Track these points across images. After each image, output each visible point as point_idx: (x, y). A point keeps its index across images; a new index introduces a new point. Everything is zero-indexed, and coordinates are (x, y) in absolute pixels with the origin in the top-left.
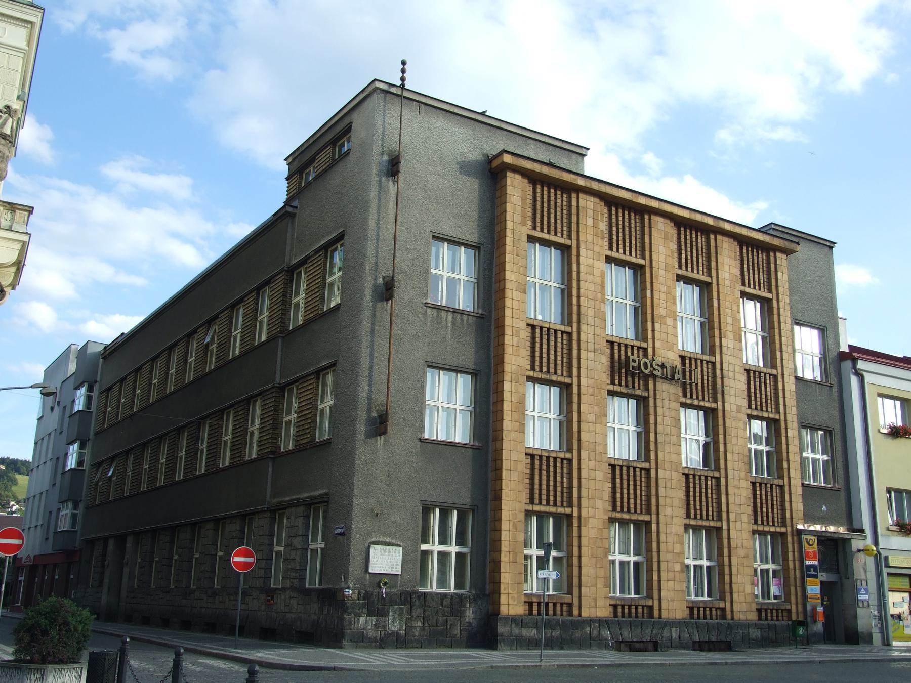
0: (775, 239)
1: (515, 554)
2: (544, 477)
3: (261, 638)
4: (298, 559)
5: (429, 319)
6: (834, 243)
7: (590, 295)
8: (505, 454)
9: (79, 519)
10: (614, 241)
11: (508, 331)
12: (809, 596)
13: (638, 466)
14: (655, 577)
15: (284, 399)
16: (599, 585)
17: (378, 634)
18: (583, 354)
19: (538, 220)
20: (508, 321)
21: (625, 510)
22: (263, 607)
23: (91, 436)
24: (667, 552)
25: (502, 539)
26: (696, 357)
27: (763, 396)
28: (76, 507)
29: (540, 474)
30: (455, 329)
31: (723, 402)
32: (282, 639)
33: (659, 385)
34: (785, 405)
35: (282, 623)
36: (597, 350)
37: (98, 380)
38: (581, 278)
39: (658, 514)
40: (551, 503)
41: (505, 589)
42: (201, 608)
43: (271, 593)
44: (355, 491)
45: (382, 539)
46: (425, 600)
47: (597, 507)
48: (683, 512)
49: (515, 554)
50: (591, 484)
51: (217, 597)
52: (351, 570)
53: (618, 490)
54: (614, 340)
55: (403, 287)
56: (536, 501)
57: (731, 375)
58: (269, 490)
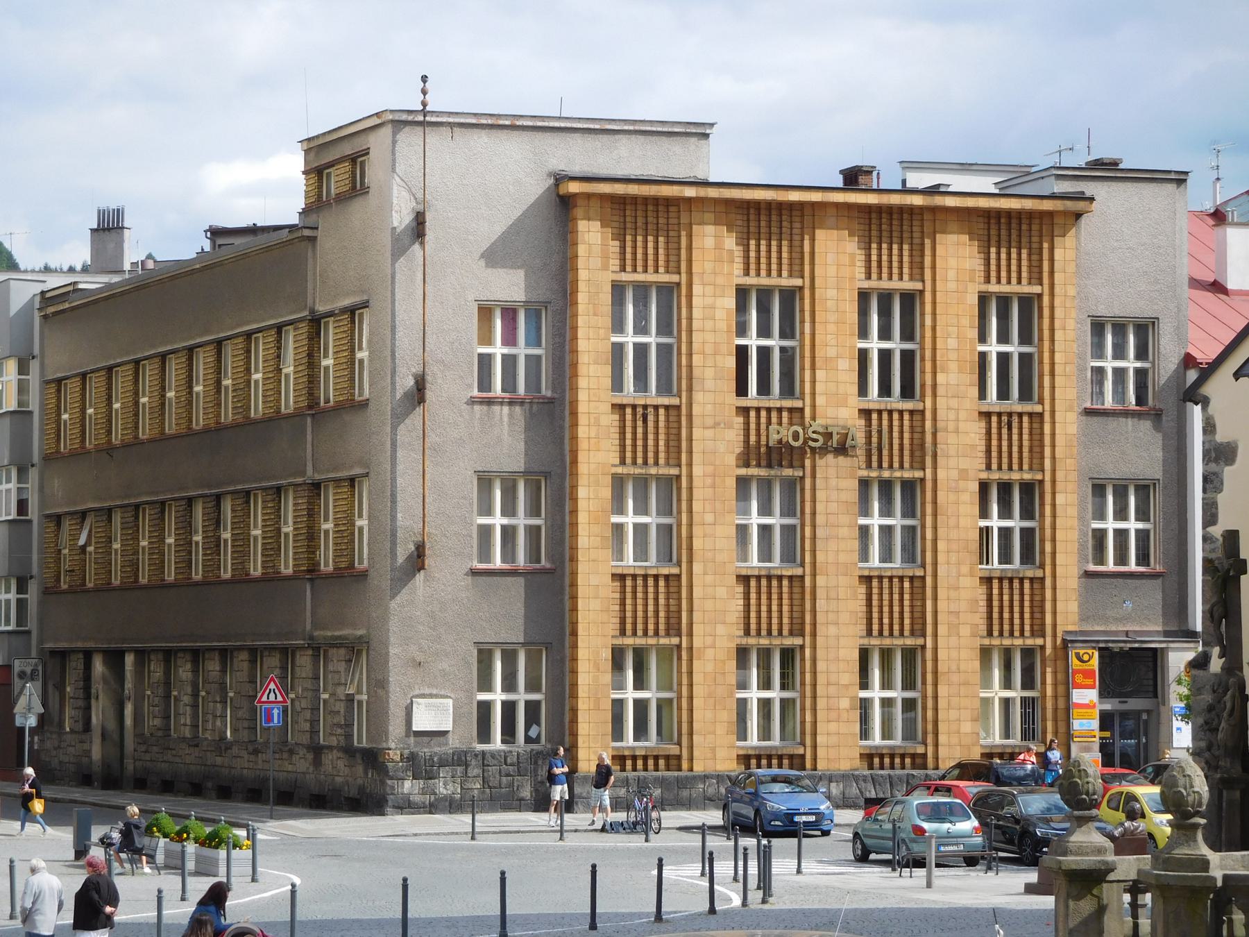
0: (1045, 201)
1: (597, 700)
2: (640, 602)
3: (311, 807)
4: (342, 711)
5: (478, 416)
6: (1186, 173)
7: (709, 349)
8: (581, 580)
9: (33, 608)
10: (752, 260)
11: (582, 419)
12: (1076, 733)
13: (785, 573)
14: (808, 718)
15: (320, 499)
16: (719, 732)
17: (427, 799)
18: (697, 433)
19: (629, 256)
20: (582, 408)
21: (764, 632)
22: (311, 769)
23: (36, 458)
24: (828, 684)
25: (579, 683)
26: (889, 408)
27: (1015, 449)
28: (22, 588)
29: (635, 598)
30: (514, 424)
31: (935, 468)
32: (332, 809)
33: (820, 462)
34: (1053, 458)
35: (330, 788)
36: (719, 424)
37: (36, 351)
38: (694, 328)
39: (814, 635)
40: (651, 632)
41: (584, 742)
42: (242, 768)
43: (317, 751)
44: (392, 639)
45: (427, 691)
46: (483, 759)
47: (718, 633)
48: (861, 628)
49: (597, 700)
50: (709, 605)
51: (260, 755)
52: (391, 728)
53: (753, 608)
54: (749, 405)
55: (440, 381)
56: (629, 632)
57: (951, 426)
58: (309, 621)
